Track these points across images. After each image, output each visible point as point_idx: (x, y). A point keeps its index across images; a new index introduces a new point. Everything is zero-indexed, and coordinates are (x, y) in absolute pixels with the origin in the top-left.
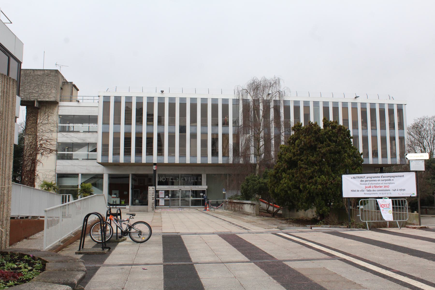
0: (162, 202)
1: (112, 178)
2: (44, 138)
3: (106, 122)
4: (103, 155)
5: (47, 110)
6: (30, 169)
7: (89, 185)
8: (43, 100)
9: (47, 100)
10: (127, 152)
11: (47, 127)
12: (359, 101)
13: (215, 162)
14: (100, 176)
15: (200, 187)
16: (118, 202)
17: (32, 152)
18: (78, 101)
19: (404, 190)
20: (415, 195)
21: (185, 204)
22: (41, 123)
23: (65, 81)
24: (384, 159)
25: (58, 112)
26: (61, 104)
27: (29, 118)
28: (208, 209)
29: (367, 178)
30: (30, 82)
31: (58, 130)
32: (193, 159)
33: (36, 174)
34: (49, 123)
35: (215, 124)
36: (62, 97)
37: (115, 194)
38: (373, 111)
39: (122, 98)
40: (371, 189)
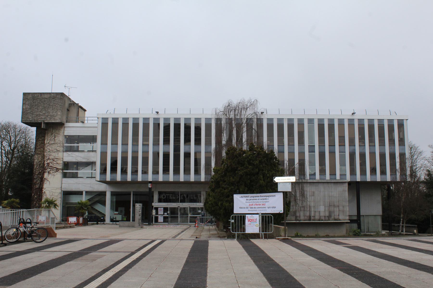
0: (161, 219)
1: (136, 195)
2: (51, 157)
3: (104, 143)
5: (54, 131)
6: (39, 187)
9: (53, 122)
10: (332, 152)
11: (54, 147)
12: (356, 117)
14: (103, 194)
17: (41, 171)
19: (275, 207)
20: (282, 212)
22: (48, 143)
24: (383, 176)
25: (64, 133)
26: (67, 125)
27: (38, 138)
29: (251, 197)
30: (37, 105)
34: (56, 143)
38: (371, 127)
40: (253, 206)
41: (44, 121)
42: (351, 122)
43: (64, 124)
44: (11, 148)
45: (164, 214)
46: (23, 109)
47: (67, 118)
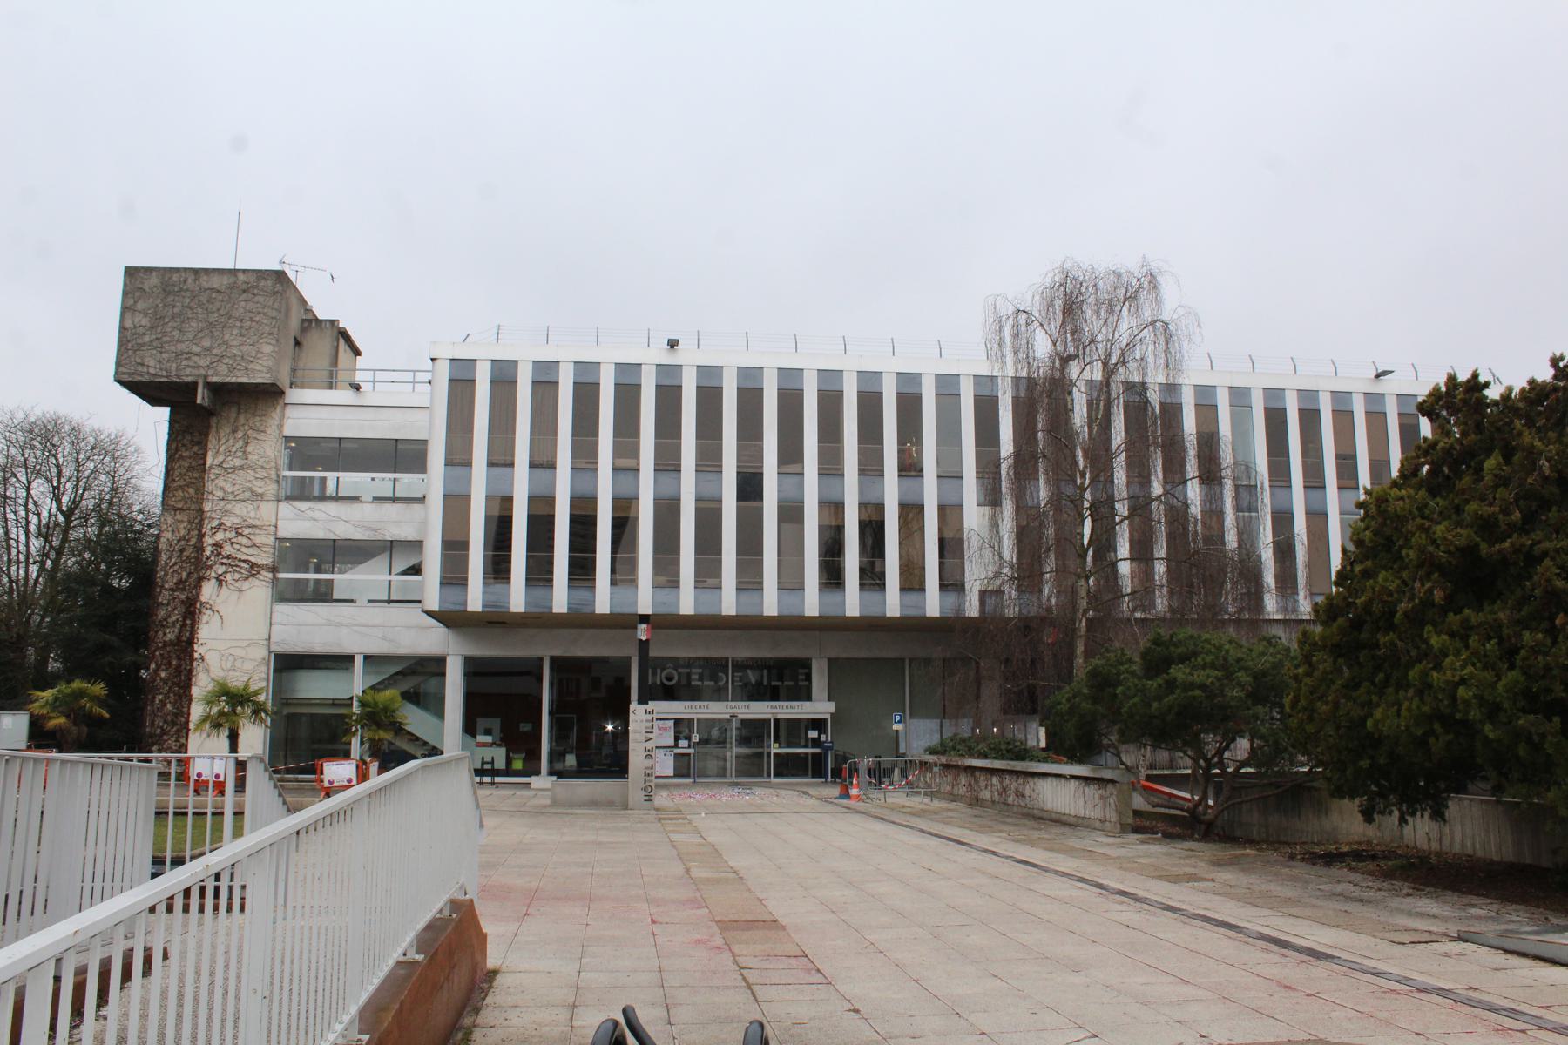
1: (476, 674)
2: (229, 521)
3: (458, 459)
4: (445, 582)
5: (242, 419)
6: (178, 638)
7: (392, 700)
8: (227, 380)
9: (244, 380)
11: (241, 478)
13: (874, 611)
14: (432, 666)
15: (807, 704)
16: (500, 764)
17: (184, 575)
18: (357, 388)
21: (752, 768)
23: (310, 317)
25: (281, 426)
26: (294, 395)
27: (177, 450)
28: (854, 792)
31: (282, 494)
32: (791, 598)
33: (196, 655)
34: (250, 467)
35: (871, 467)
36: (300, 373)
37: (488, 732)
39: (520, 366)
41: (205, 377)
42: (1374, 398)
43: (282, 393)
44: (59, 509)
45: (676, 746)
46: (122, 329)
47: (294, 371)
